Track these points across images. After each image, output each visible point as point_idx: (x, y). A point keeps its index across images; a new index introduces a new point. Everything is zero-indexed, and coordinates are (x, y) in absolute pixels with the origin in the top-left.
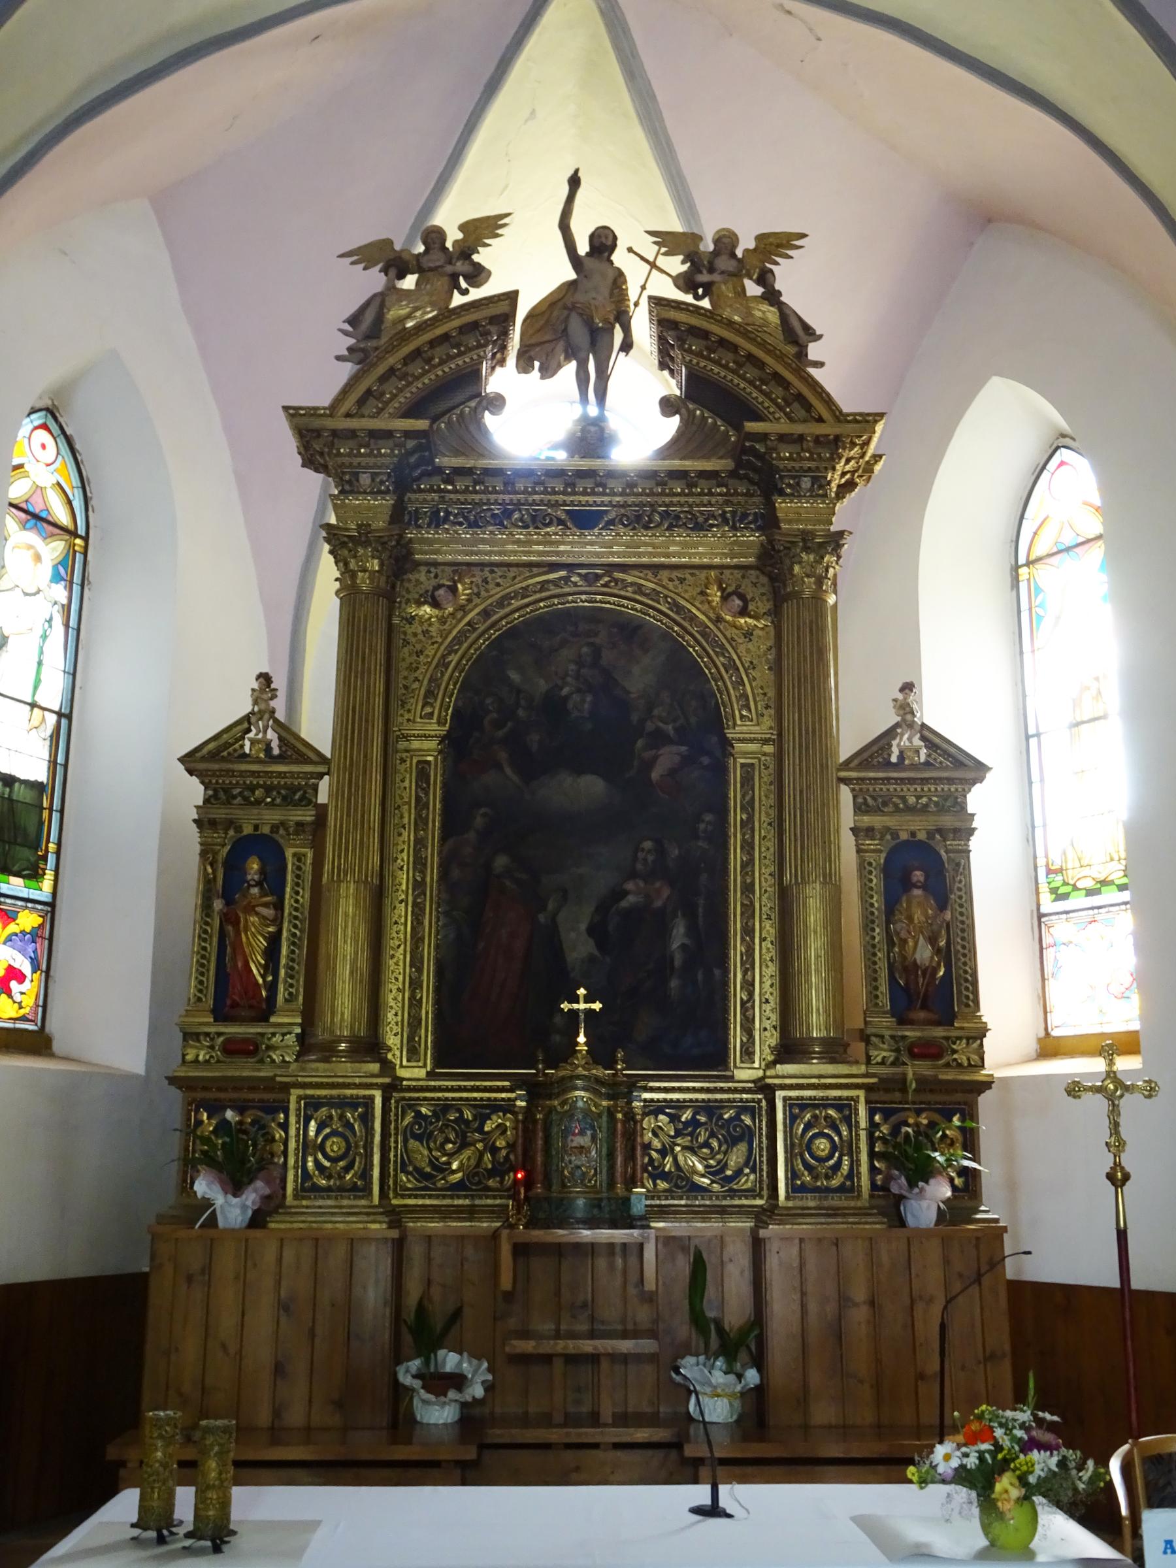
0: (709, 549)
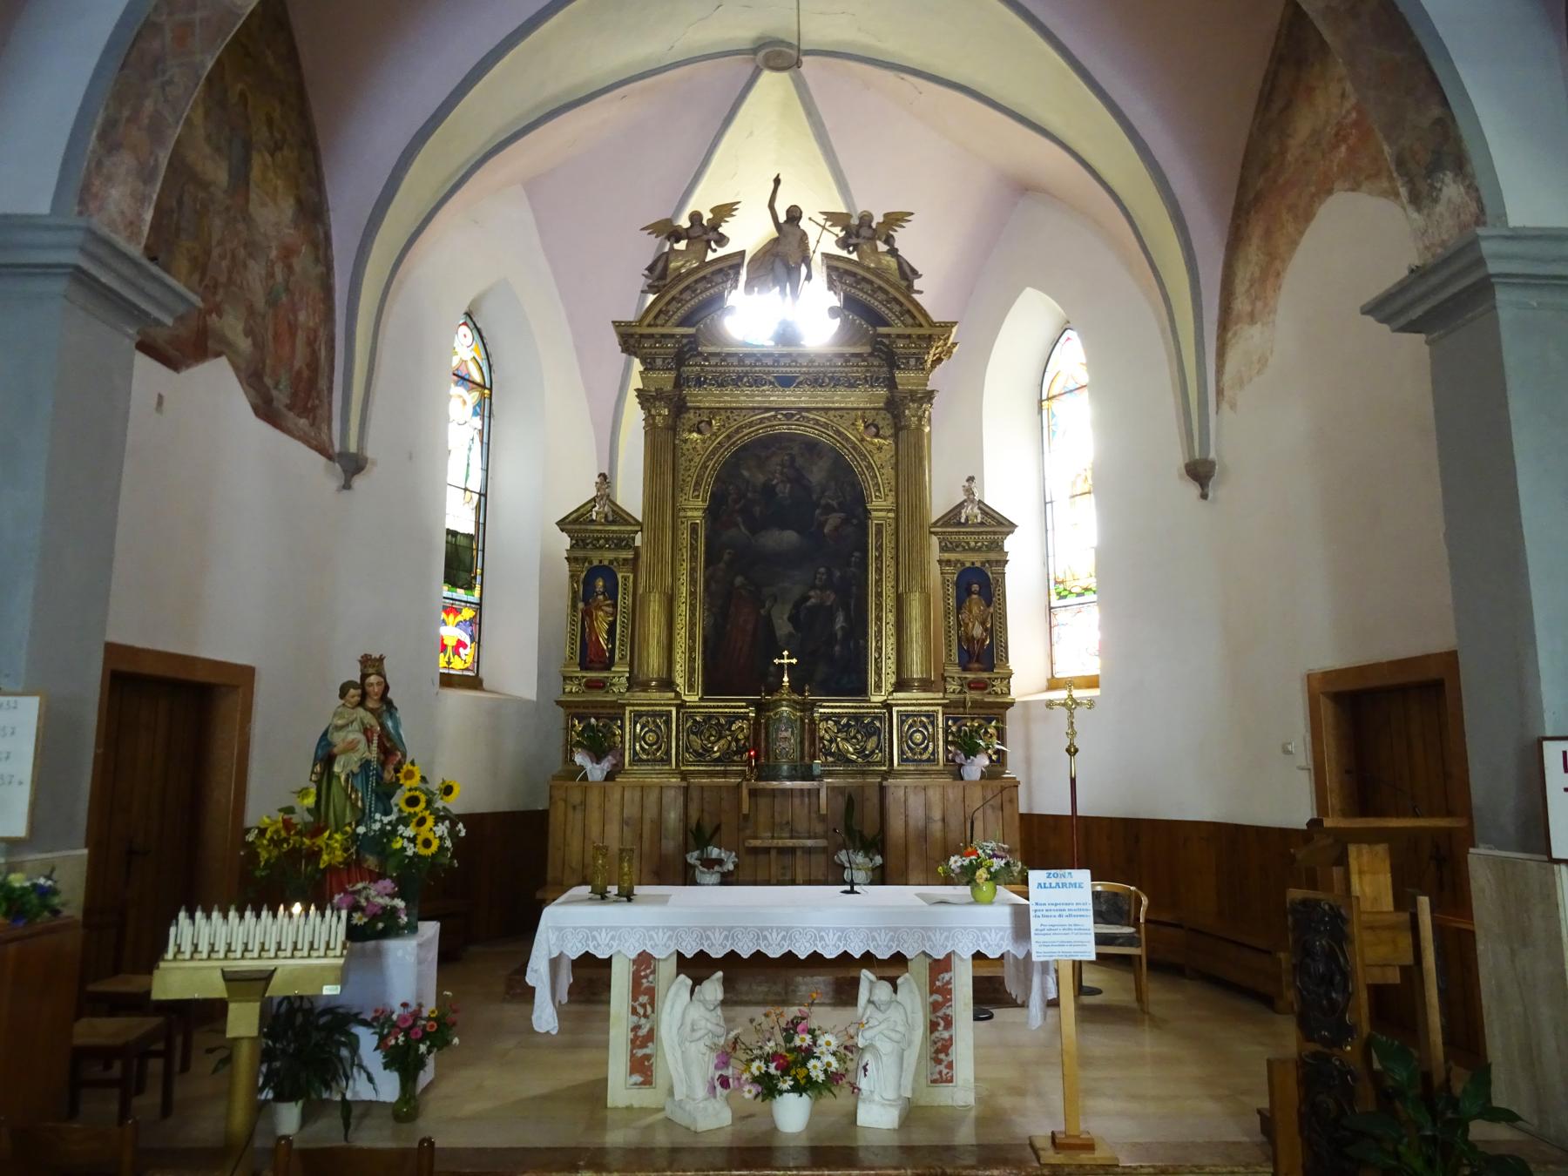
0: (856, 398)
